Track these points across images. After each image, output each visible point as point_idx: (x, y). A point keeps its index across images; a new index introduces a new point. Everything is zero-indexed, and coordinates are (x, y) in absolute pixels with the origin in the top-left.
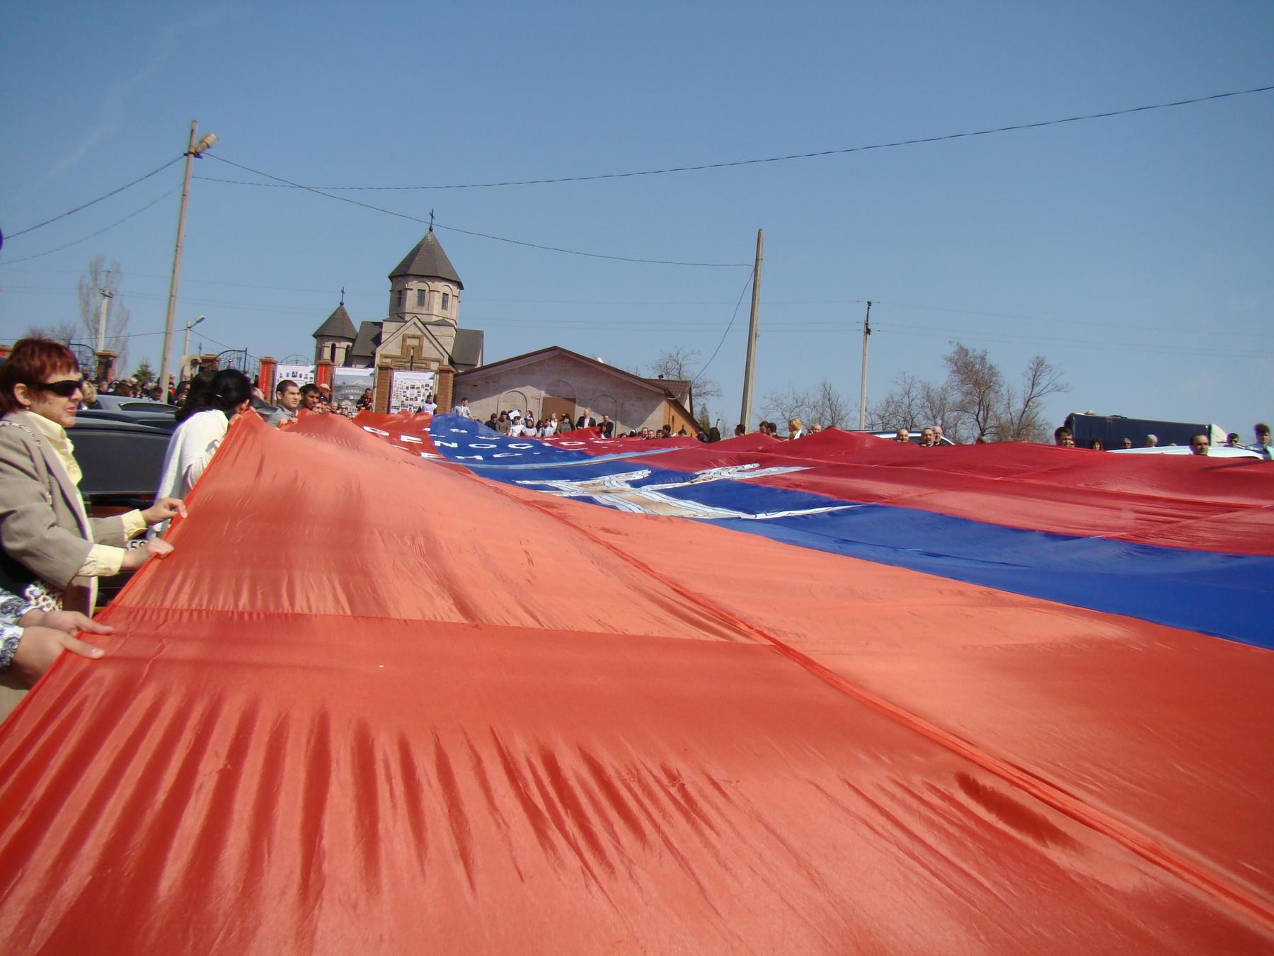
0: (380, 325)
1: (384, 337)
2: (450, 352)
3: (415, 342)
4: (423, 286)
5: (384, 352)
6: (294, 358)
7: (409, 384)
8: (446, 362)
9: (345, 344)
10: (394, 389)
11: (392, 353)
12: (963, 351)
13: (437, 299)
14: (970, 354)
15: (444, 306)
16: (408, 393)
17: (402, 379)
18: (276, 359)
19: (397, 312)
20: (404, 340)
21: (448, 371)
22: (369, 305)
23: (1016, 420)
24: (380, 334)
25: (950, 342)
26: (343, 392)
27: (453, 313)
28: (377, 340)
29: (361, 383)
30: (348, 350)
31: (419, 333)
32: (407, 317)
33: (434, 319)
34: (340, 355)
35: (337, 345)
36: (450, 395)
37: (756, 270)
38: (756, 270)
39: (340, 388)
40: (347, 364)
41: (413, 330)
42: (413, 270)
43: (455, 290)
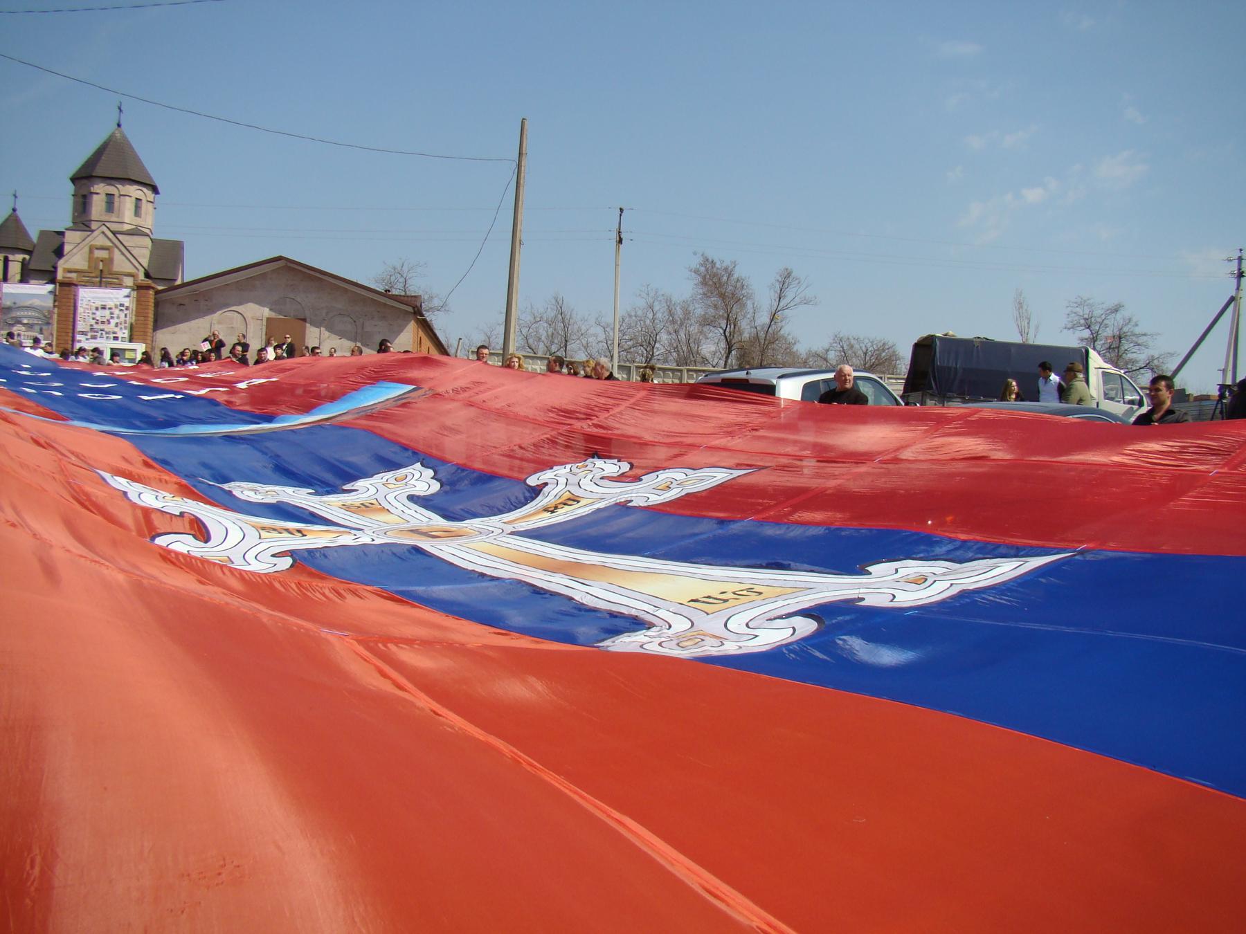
1: (67, 248)
2: (146, 265)
3: (104, 254)
4: (111, 190)
5: (68, 266)
7: (99, 303)
8: (141, 276)
9: (20, 257)
10: (80, 310)
11: (78, 267)
12: (708, 263)
13: (129, 205)
14: (718, 265)
16: (99, 314)
17: (88, 297)
19: (82, 220)
20: (91, 251)
21: (148, 288)
23: (762, 335)
25: (695, 254)
26: (14, 314)
28: (59, 252)
29: (37, 302)
30: (24, 264)
31: (109, 244)
32: (94, 226)
33: (126, 227)
34: (15, 269)
35: (11, 257)
36: (151, 316)
37: (519, 166)
38: (519, 166)
40: (24, 280)
42: (99, 171)
43: (150, 195)
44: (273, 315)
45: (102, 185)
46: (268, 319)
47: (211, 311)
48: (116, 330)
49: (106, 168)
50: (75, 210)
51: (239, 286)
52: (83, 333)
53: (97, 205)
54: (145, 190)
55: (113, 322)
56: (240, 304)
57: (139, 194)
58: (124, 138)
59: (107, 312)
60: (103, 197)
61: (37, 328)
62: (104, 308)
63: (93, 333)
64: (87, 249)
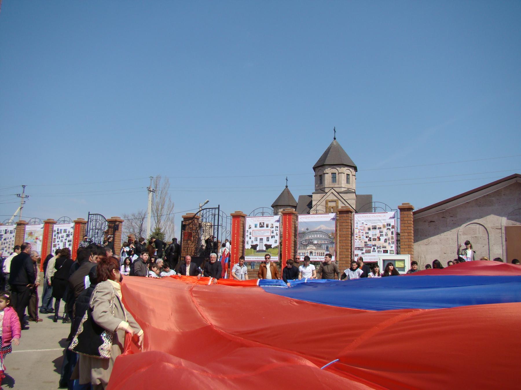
0: (311, 196)
1: (314, 203)
4: (334, 171)
6: (261, 210)
7: (370, 225)
13: (343, 177)
15: (348, 181)
16: (371, 233)
17: (360, 220)
18: (245, 213)
19: (320, 188)
20: (326, 203)
22: (303, 186)
24: (311, 202)
27: (353, 186)
29: (323, 227)
31: (335, 198)
32: (327, 190)
33: (343, 190)
39: (304, 233)
41: (331, 197)
44: (511, 223)
45: (329, 169)
46: (506, 228)
47: (457, 224)
48: (386, 244)
49: (329, 162)
50: (316, 183)
51: (478, 203)
52: (359, 249)
53: (328, 178)
54: (351, 169)
55: (382, 239)
56: (481, 217)
57: (348, 172)
58: (339, 145)
59: (377, 231)
60: (330, 175)
61: (324, 247)
62: (375, 228)
63: (367, 248)
64: (324, 203)
